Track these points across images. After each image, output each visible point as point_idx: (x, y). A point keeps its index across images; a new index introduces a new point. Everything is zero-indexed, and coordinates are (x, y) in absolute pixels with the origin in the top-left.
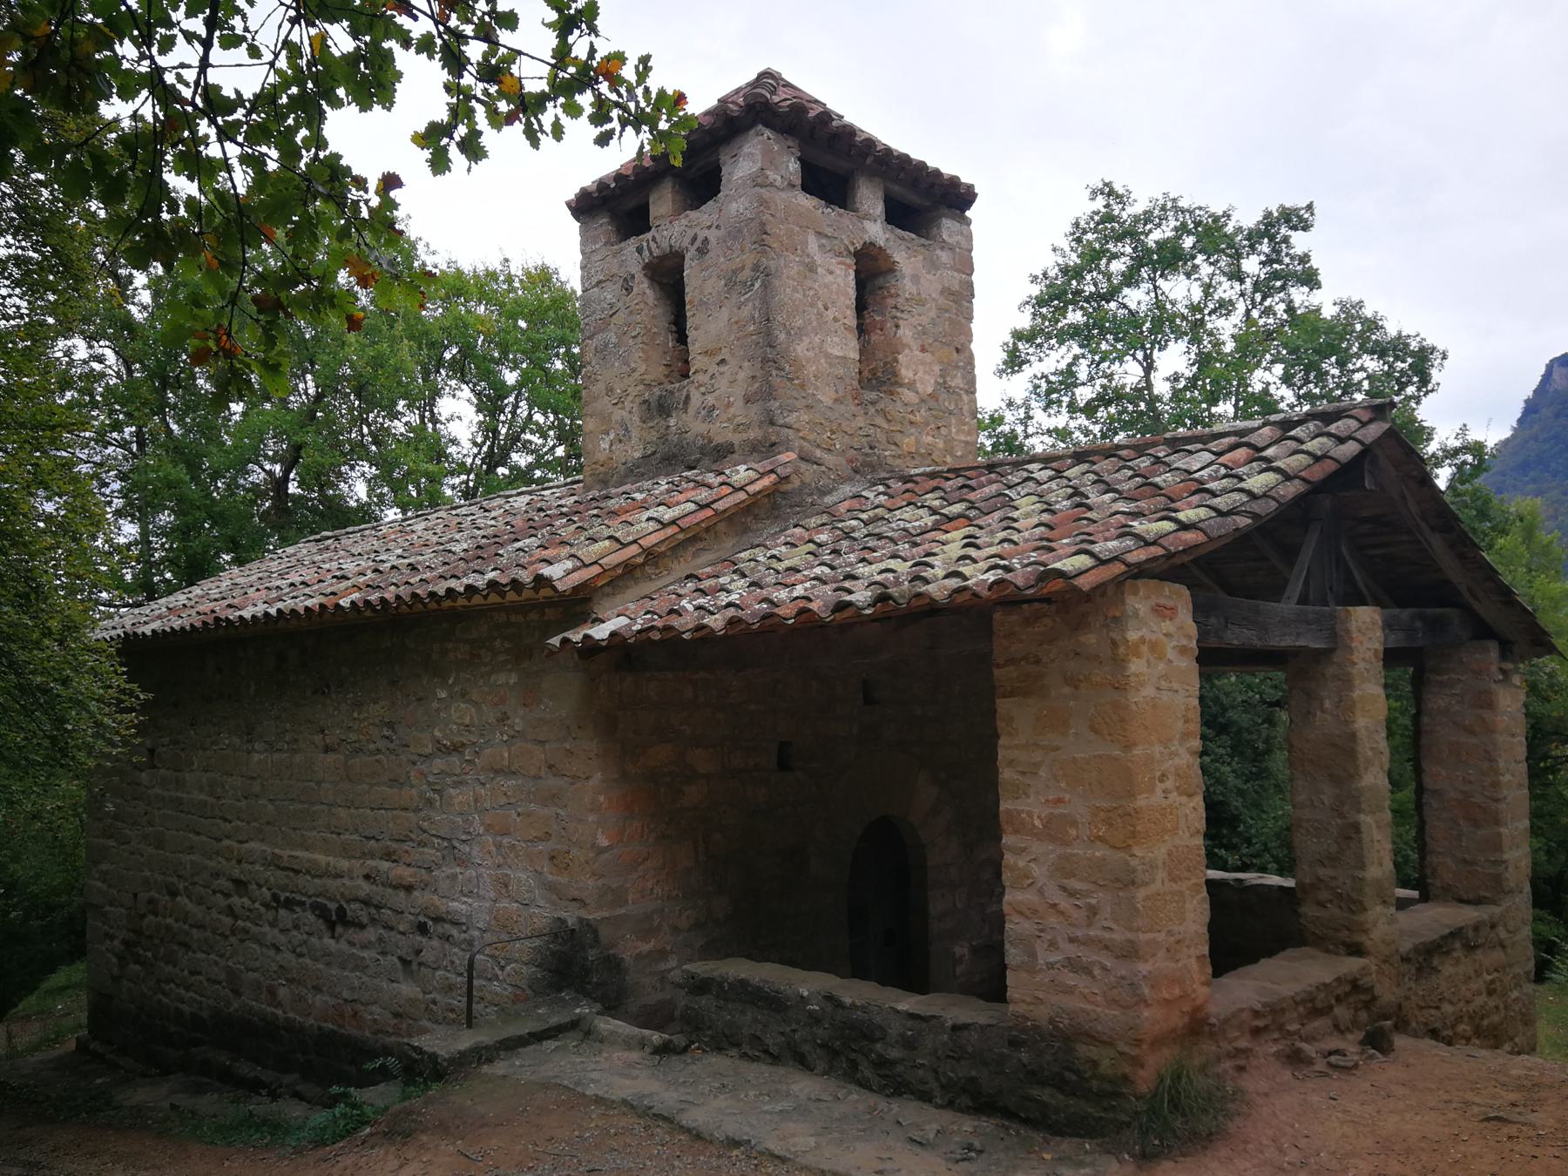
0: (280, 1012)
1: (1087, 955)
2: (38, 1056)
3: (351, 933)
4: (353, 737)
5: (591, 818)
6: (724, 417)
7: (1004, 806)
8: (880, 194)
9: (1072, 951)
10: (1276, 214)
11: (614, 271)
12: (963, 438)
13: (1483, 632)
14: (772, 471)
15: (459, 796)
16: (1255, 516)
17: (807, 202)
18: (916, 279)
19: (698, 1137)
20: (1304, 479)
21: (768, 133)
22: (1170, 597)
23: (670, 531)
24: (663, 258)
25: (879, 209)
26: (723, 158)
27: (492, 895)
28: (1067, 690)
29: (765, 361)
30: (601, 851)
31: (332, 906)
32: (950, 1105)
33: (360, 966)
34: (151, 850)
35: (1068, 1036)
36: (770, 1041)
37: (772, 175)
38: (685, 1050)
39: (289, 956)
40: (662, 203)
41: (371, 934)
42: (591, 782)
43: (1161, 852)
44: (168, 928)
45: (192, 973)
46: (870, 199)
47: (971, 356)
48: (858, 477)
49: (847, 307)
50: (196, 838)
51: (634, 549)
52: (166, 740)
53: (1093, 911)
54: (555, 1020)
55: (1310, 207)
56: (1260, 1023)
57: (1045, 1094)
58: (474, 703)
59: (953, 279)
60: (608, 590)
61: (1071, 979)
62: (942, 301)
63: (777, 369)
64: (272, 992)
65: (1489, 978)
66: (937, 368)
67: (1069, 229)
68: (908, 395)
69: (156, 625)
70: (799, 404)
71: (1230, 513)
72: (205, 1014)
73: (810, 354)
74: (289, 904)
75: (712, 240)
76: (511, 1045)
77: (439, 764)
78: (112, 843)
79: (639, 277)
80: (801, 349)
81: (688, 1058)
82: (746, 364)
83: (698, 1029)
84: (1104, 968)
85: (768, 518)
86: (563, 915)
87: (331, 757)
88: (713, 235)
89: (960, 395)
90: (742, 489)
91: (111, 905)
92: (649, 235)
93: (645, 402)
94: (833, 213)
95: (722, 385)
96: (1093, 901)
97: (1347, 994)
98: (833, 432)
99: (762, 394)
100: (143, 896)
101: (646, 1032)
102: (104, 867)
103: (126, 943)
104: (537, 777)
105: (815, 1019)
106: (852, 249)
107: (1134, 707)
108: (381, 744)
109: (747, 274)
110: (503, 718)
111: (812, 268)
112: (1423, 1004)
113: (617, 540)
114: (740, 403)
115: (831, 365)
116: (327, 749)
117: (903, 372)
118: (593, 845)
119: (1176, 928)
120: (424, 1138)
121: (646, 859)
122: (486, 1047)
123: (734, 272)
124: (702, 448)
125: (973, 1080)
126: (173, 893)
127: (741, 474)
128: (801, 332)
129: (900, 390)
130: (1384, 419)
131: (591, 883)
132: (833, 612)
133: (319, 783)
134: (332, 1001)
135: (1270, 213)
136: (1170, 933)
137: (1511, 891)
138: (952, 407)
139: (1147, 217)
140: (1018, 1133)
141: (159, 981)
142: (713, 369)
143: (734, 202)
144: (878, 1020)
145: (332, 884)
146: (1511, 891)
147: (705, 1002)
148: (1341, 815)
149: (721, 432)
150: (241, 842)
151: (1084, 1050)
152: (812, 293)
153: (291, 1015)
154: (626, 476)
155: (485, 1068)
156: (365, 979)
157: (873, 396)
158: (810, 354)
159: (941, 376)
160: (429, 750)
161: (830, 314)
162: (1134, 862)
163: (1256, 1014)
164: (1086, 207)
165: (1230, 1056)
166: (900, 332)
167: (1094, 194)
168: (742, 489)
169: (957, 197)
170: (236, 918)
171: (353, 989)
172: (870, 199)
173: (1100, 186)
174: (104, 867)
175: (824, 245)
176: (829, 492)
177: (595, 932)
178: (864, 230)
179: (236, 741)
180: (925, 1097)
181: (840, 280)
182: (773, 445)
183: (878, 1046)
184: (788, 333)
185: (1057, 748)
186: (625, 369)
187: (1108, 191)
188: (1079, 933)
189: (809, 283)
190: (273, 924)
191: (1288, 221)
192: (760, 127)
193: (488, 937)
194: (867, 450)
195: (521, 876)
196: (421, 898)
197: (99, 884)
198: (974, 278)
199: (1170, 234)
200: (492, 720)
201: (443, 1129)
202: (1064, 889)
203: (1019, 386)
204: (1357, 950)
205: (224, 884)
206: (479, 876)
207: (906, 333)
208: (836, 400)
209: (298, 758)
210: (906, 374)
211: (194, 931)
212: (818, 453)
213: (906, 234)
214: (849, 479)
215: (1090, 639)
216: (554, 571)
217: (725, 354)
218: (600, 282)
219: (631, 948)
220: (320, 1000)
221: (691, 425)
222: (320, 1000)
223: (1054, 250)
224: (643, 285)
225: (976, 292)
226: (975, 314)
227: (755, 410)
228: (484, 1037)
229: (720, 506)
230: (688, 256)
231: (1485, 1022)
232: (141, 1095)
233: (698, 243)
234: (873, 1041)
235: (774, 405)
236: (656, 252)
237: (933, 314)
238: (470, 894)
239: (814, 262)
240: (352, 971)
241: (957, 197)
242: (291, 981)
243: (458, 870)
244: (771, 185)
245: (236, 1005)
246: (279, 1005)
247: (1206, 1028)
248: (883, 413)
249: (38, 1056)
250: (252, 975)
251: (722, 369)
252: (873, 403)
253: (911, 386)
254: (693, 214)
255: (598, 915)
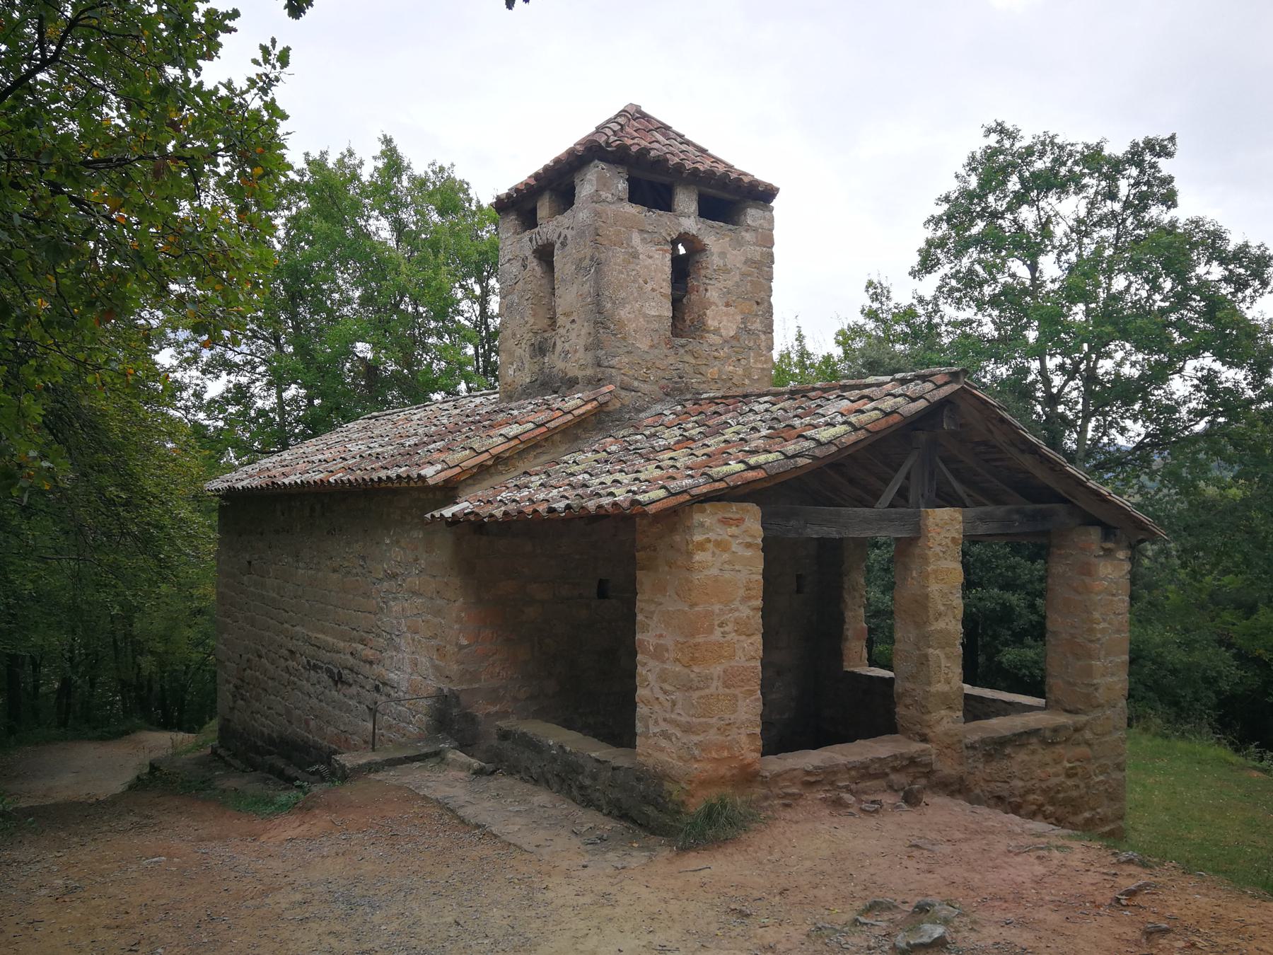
0: (311, 737)
1: (672, 730)
2: (189, 755)
3: (345, 689)
4: (346, 564)
5: (456, 626)
6: (573, 360)
7: (638, 636)
8: (695, 197)
9: (664, 726)
10: (1142, 145)
11: (518, 253)
12: (760, 366)
13: (1091, 521)
14: (594, 399)
15: (396, 607)
16: (814, 458)
17: (632, 209)
18: (723, 255)
19: (463, 821)
20: (867, 430)
21: (602, 165)
22: (737, 513)
23: (513, 443)
24: (544, 246)
25: (693, 207)
26: (577, 181)
27: (410, 670)
28: (667, 568)
29: (596, 323)
30: (461, 647)
31: (336, 671)
32: (609, 814)
33: (349, 710)
34: (248, 626)
35: (661, 777)
36: (533, 771)
37: (604, 194)
38: (492, 773)
39: (315, 701)
40: (543, 209)
41: (354, 690)
42: (457, 604)
43: (717, 670)
44: (257, 678)
45: (269, 708)
46: (686, 202)
47: (770, 306)
48: (668, 398)
49: (664, 280)
50: (271, 621)
51: (486, 456)
52: (256, 556)
53: (674, 704)
54: (425, 750)
55: (1172, 138)
56: (812, 779)
57: (649, 810)
58: (403, 549)
59: (755, 252)
60: (470, 481)
61: (664, 743)
62: (745, 269)
63: (604, 328)
64: (307, 723)
65: (1068, 765)
66: (739, 318)
67: (966, 161)
68: (713, 338)
69: (244, 483)
70: (620, 351)
71: (794, 456)
72: (275, 735)
73: (632, 316)
74: (315, 667)
75: (569, 237)
76: (393, 763)
77: (386, 585)
78: (228, 620)
79: (531, 258)
80: (623, 313)
81: (491, 778)
82: (586, 324)
83: (501, 761)
84: (677, 737)
85: (594, 430)
86: (442, 686)
87: (335, 576)
88: (569, 233)
89: (758, 336)
90: (570, 412)
91: (228, 660)
92: (536, 230)
93: (532, 344)
94: (655, 215)
95: (573, 335)
96: (674, 697)
97: (907, 766)
98: (648, 369)
99: (595, 345)
100: (245, 657)
101: (473, 760)
102: (225, 636)
103: (236, 687)
104: (431, 598)
105: (554, 759)
106: (669, 239)
107: (697, 582)
108: (359, 570)
109: (587, 262)
110: (416, 560)
111: (635, 255)
112: (989, 779)
113: (474, 450)
114: (582, 350)
115: (648, 322)
116: (335, 571)
117: (710, 322)
118: (457, 644)
119: (727, 716)
120: (317, 812)
121: (495, 654)
122: (376, 763)
123: (580, 260)
124: (562, 378)
125: (618, 800)
126: (260, 656)
127: (573, 401)
128: (624, 302)
129: (707, 335)
130: (957, 382)
131: (455, 667)
132: (548, 512)
133: (330, 591)
134: (336, 731)
135: (1137, 144)
136: (721, 719)
137: (1099, 706)
138: (751, 344)
139: (1029, 151)
140: (634, 832)
141: (252, 713)
142: (568, 326)
143: (581, 213)
144: (581, 761)
145: (336, 656)
146: (1099, 706)
147: (507, 745)
148: (919, 649)
149: (573, 371)
150: (293, 626)
151: (668, 786)
152: (634, 273)
153: (316, 738)
154: (522, 394)
155: (372, 776)
156: (351, 718)
157: (683, 341)
158: (632, 316)
159: (742, 323)
160: (381, 576)
161: (649, 287)
162: (693, 676)
163: (808, 773)
164: (980, 143)
165: (779, 797)
166: (708, 294)
167: (989, 131)
168: (570, 412)
169: (763, 195)
170: (290, 674)
171: (345, 724)
172: (686, 202)
173: (994, 125)
174: (225, 636)
175: (645, 239)
176: (644, 410)
177: (457, 697)
178: (680, 225)
179: (290, 560)
180: (599, 809)
181: (658, 262)
182: (599, 380)
183: (580, 777)
184: (614, 303)
185: (661, 604)
186: (522, 321)
187: (1001, 130)
188: (668, 716)
189: (631, 266)
190: (308, 680)
191: (1152, 149)
192: (596, 161)
193: (407, 696)
194: (677, 379)
195: (423, 660)
196: (377, 669)
197: (222, 647)
198: (775, 250)
199: (1049, 165)
200: (411, 560)
201: (328, 807)
202: (661, 688)
203: (929, 285)
204: (924, 739)
205: (284, 652)
206: (403, 658)
207: (713, 295)
208: (651, 347)
209: (320, 574)
210: (712, 323)
211: (270, 681)
212: (636, 384)
213: (716, 224)
214: (661, 401)
215: (677, 538)
216: (428, 471)
217: (575, 316)
218: (509, 260)
219: (481, 709)
220: (330, 730)
221: (556, 362)
222: (330, 730)
223: (957, 177)
224: (533, 264)
225: (775, 260)
226: (775, 275)
227: (588, 358)
228: (377, 757)
229: (552, 425)
230: (556, 246)
231: (1061, 795)
232: (232, 783)
233: (561, 238)
234: (578, 774)
235: (601, 353)
236: (540, 242)
237: (737, 278)
238: (399, 669)
239: (637, 251)
240: (345, 712)
241: (763, 195)
242: (316, 717)
243: (394, 653)
244: (604, 201)
245: (290, 731)
246: (310, 732)
247: (760, 779)
248: (692, 353)
249: (189, 755)
250: (298, 712)
251: (573, 326)
252: (683, 346)
253: (716, 331)
254: (559, 218)
255: (459, 688)
